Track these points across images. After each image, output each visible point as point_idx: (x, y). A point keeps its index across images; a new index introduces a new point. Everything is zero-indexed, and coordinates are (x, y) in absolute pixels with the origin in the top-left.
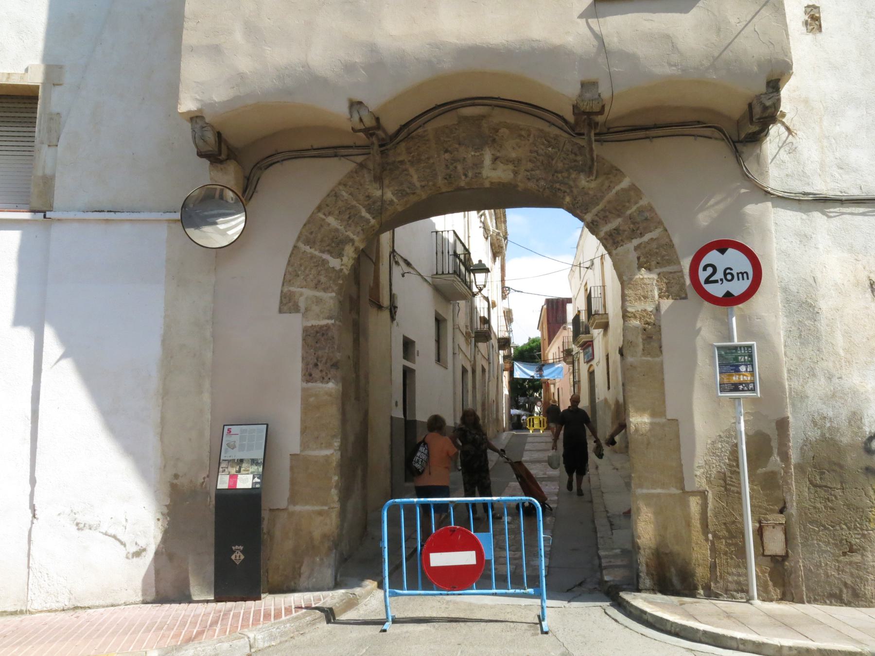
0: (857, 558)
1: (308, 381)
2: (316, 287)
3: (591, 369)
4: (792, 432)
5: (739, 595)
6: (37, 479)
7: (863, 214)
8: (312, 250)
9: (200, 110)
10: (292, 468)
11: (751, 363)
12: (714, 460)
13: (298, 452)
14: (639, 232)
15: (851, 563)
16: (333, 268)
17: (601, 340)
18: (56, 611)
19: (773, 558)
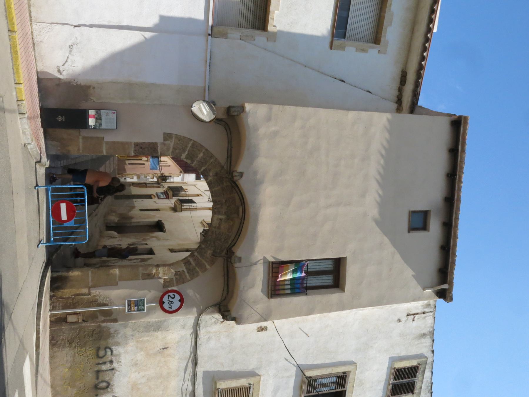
0: (67, 345)
1: (134, 144)
2: (174, 148)
3: (153, 196)
4: (113, 324)
5: (51, 307)
6: (92, 28)
7: (191, 345)
8: (189, 147)
9: (245, 112)
10: (98, 137)
11: (138, 310)
12: (102, 298)
13: (105, 140)
14: (189, 271)
15: (65, 343)
16: (182, 155)
17: (168, 205)
18: (32, 35)
19: (66, 318)
